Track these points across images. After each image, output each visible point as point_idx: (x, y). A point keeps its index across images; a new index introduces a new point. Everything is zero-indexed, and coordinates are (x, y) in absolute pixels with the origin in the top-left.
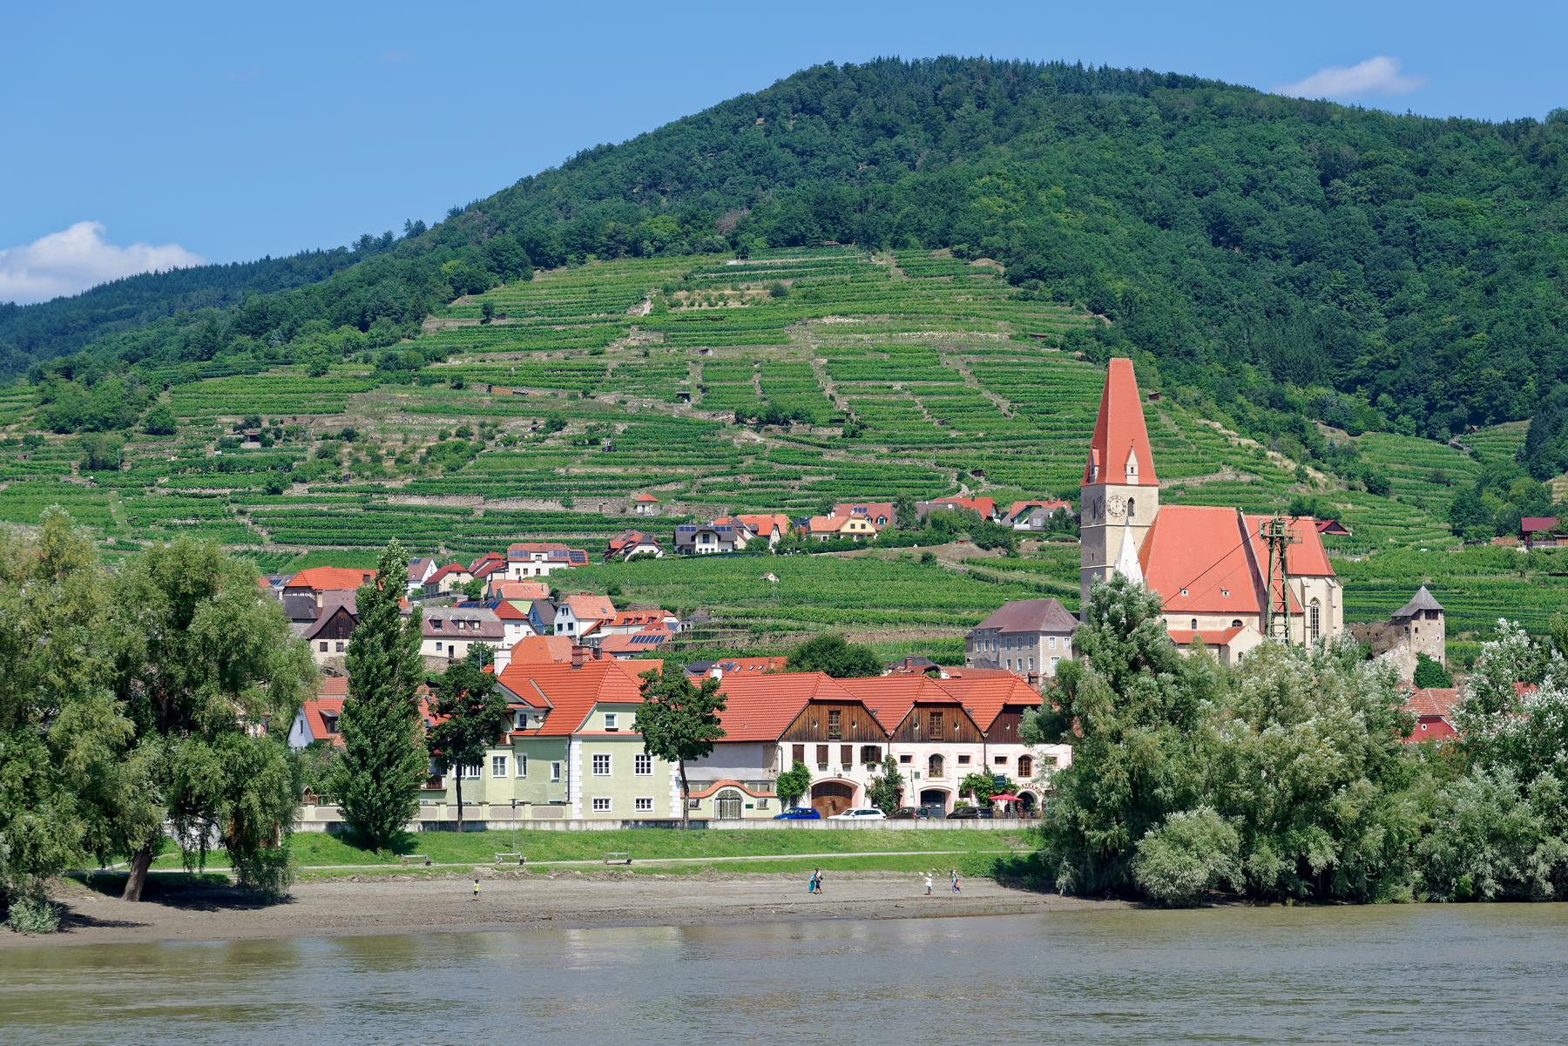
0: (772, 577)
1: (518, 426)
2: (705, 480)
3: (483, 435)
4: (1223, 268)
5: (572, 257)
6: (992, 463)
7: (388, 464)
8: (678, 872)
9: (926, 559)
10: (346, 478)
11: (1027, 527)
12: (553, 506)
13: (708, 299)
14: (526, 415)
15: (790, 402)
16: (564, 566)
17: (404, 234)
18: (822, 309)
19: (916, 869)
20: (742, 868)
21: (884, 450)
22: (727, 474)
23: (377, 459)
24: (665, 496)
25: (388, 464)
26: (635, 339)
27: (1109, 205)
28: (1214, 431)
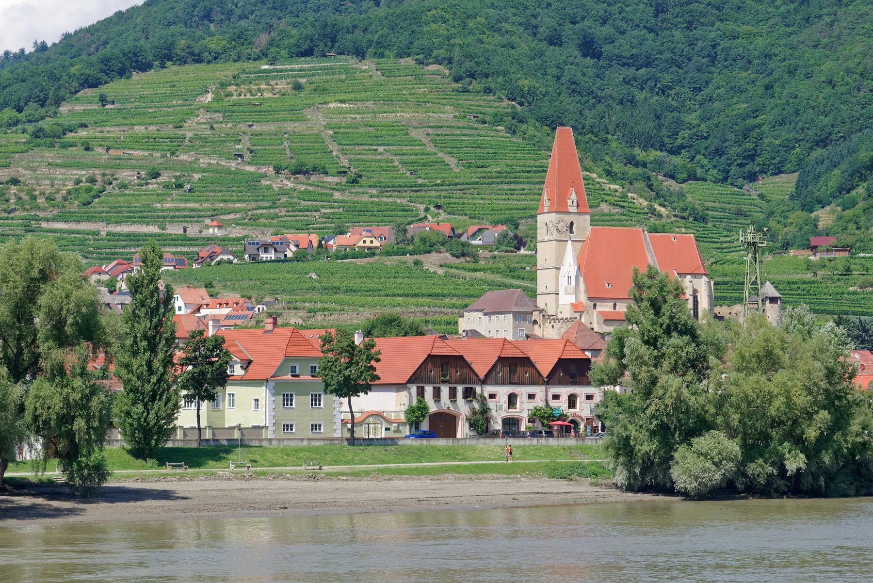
0: (314, 276)
1: (126, 175)
2: (255, 212)
3: (104, 181)
4: (591, 72)
5: (156, 63)
6: (447, 200)
7: (41, 201)
8: (356, 475)
9: (417, 263)
10: (13, 210)
11: (481, 242)
12: (153, 229)
13: (250, 92)
14: (132, 168)
15: (310, 161)
16: (171, 268)
17: (33, 50)
18: (328, 98)
19: (514, 472)
20: (399, 472)
21: (374, 192)
22: (270, 208)
23: (34, 198)
24: (229, 223)
25: (41, 201)
26: (203, 117)
27: (514, 29)
28: (593, 180)
